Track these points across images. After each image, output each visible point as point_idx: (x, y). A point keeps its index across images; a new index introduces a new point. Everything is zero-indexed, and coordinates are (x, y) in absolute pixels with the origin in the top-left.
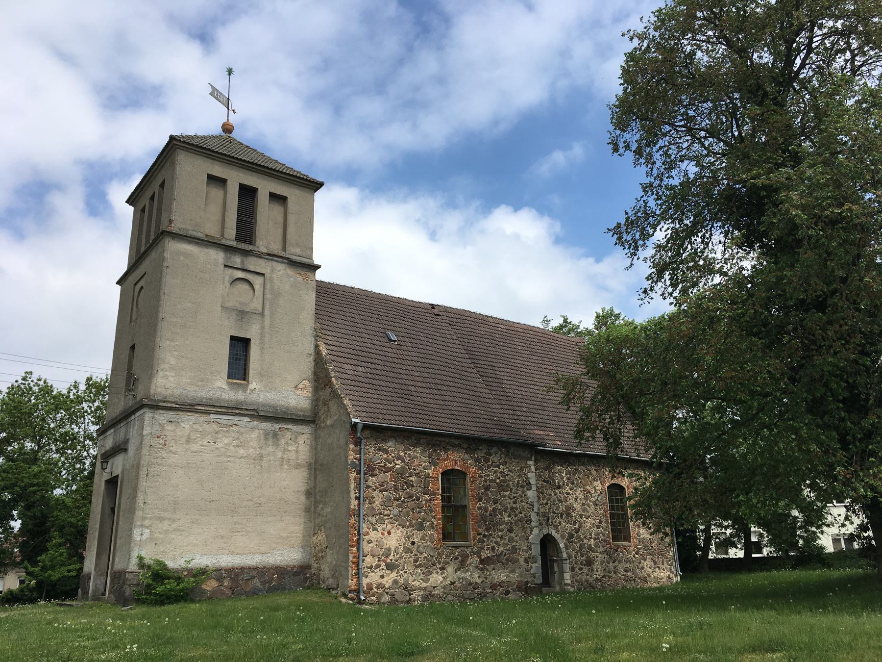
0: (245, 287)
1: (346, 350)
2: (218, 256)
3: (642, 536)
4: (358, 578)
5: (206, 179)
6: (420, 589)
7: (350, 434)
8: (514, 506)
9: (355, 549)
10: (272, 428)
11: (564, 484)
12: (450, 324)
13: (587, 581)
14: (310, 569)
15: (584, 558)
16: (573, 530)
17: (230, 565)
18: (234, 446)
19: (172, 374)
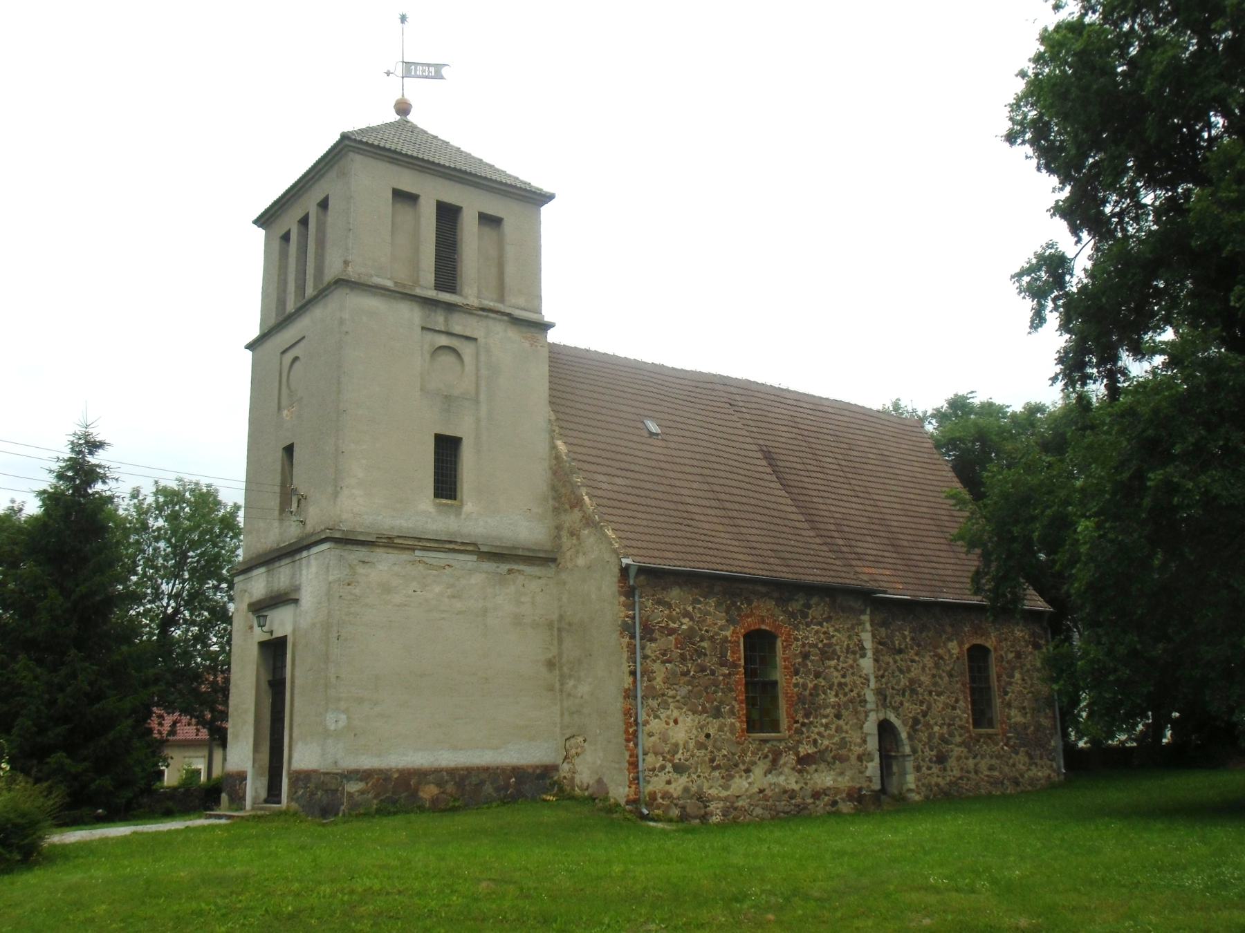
0: (448, 359)
1: (594, 452)
2: (411, 315)
3: (1013, 720)
4: (638, 784)
5: (390, 196)
6: (719, 799)
8: (843, 680)
11: (906, 647)
12: (730, 404)
13: (937, 785)
15: (934, 753)
16: (918, 713)
18: (448, 597)
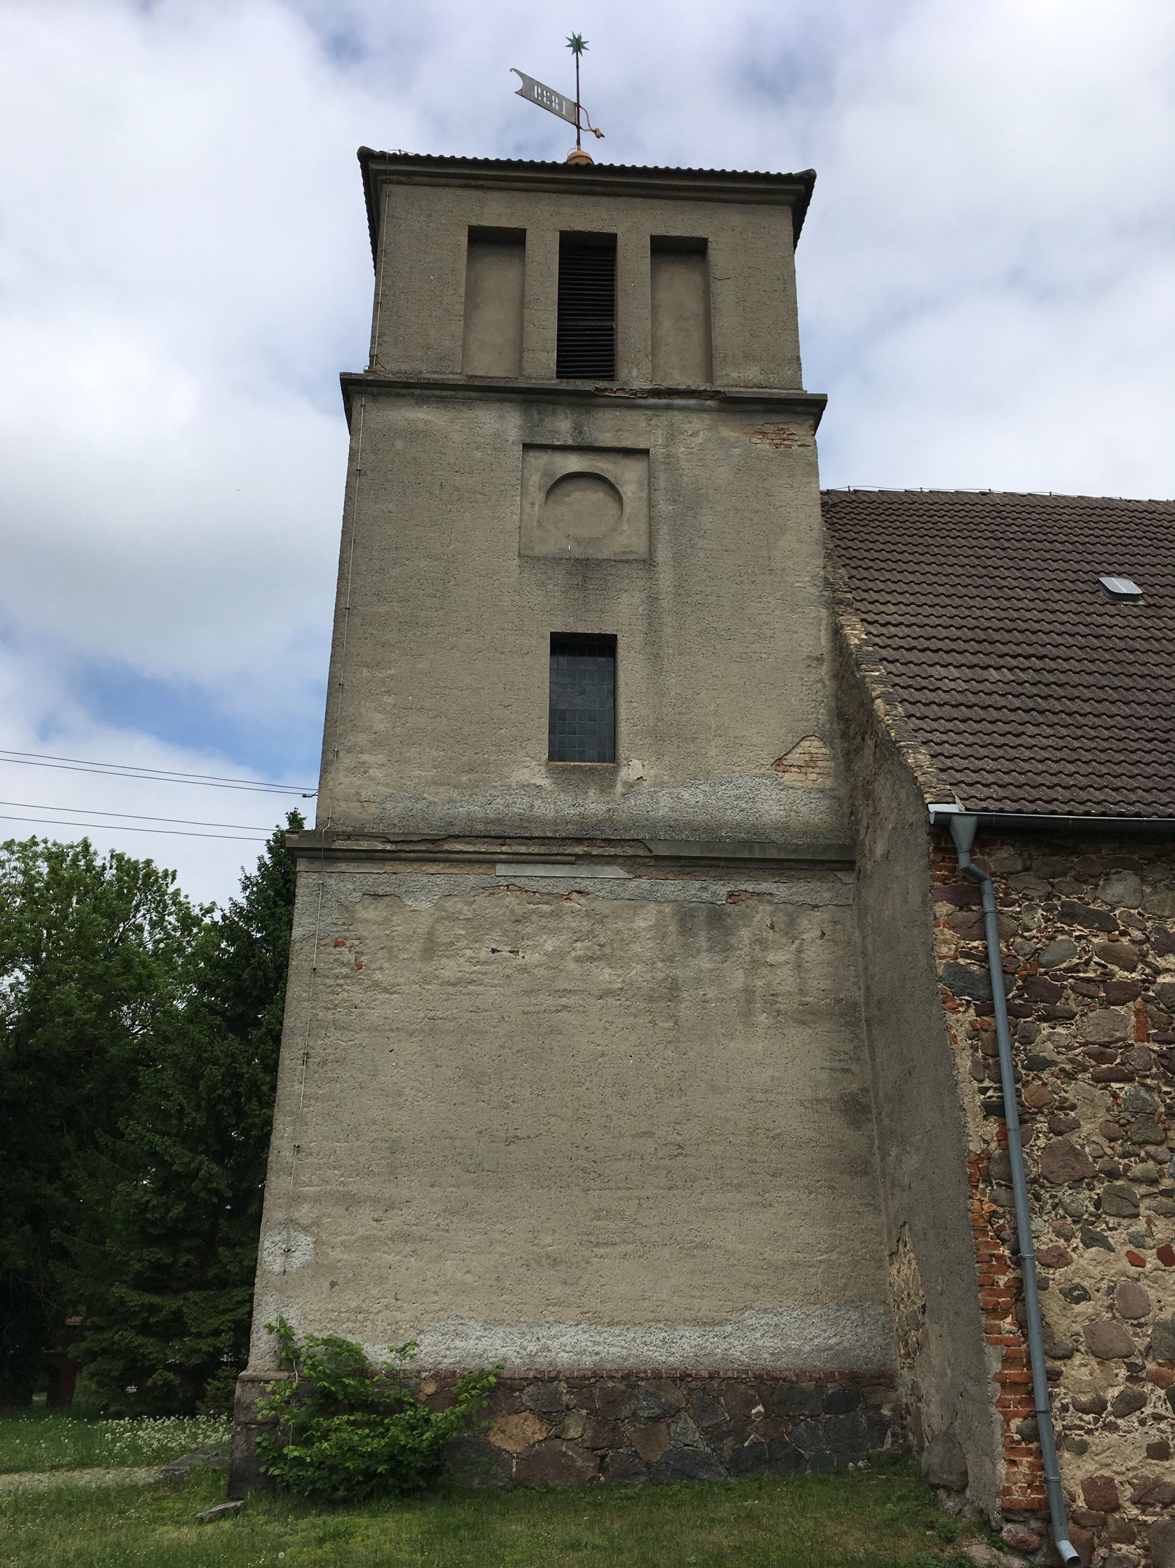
0: (593, 496)
4: (1039, 1453)
5: (464, 240)
7: (932, 865)
9: (1007, 1323)
10: (705, 896)
14: (894, 1388)
17: (588, 1361)
18: (578, 960)
19: (381, 758)
